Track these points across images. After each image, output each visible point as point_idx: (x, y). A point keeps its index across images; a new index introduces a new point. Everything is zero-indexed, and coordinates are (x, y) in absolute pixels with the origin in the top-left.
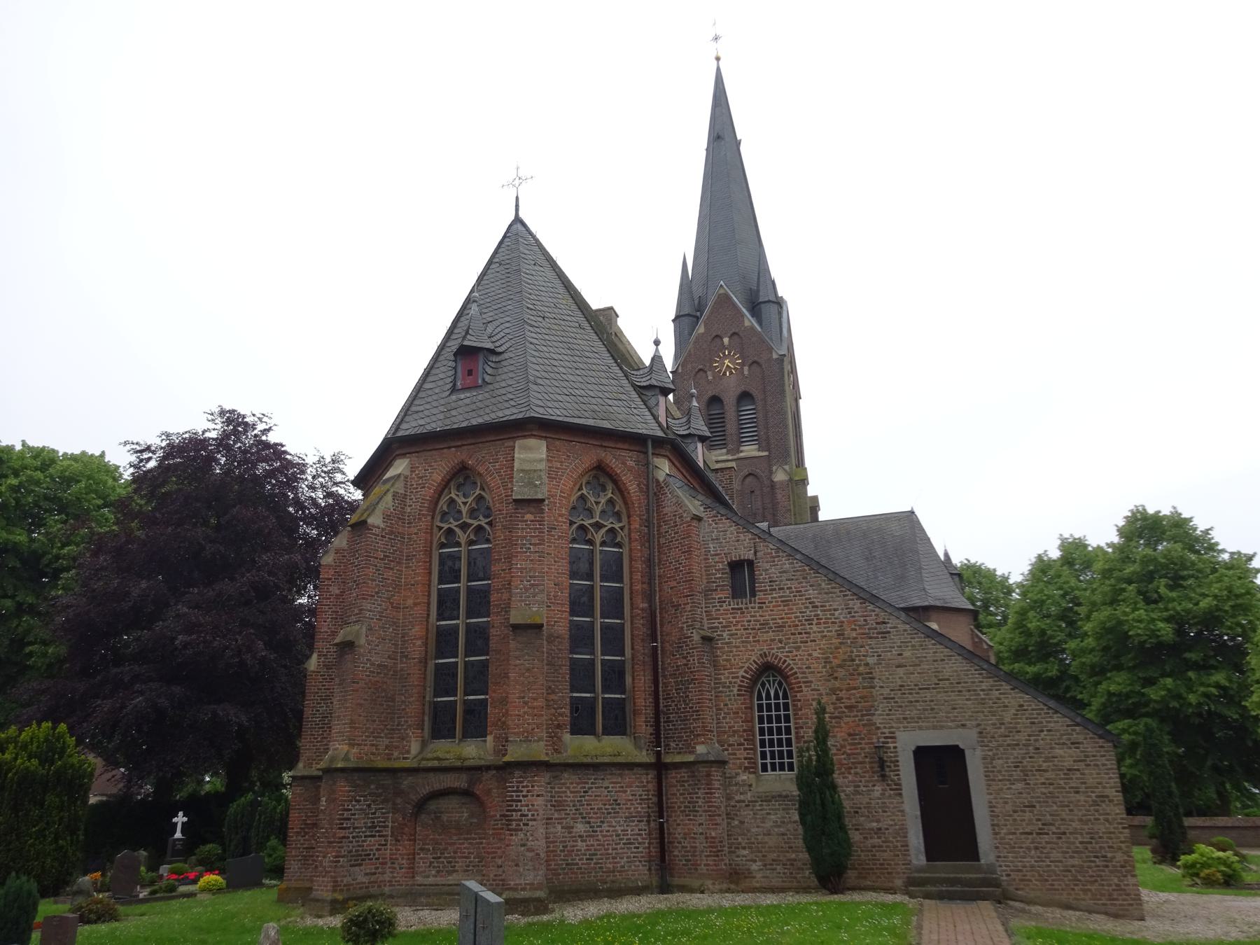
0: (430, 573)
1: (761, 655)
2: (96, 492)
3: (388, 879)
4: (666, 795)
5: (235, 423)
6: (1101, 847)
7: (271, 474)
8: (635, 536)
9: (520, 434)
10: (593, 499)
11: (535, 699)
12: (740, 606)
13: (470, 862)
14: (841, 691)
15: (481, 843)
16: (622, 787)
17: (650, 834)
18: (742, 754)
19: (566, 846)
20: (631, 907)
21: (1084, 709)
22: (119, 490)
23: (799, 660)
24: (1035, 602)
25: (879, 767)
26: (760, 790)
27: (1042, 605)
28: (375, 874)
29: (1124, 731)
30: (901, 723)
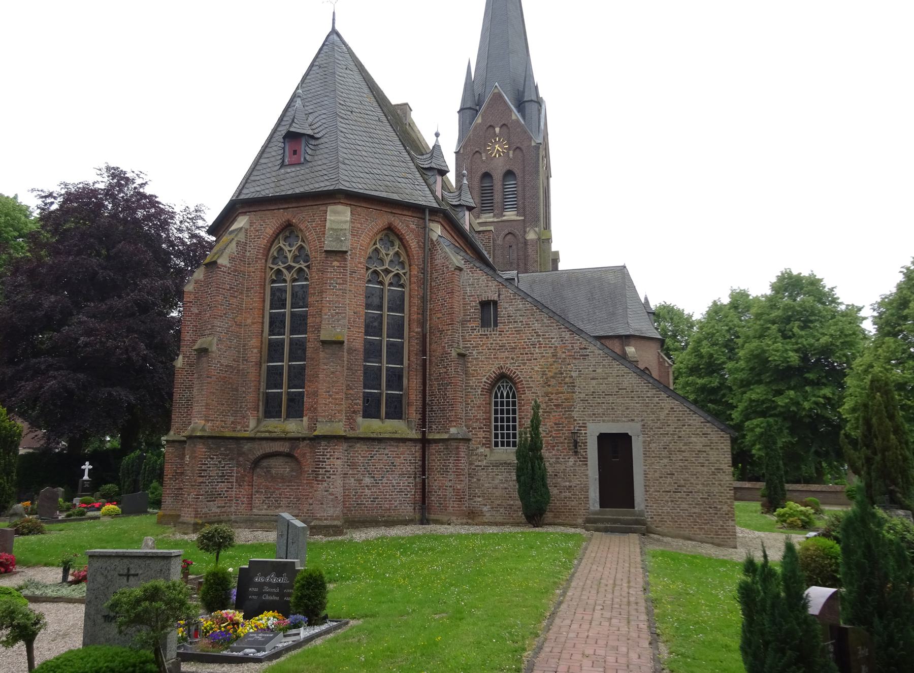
0: (264, 301)
1: (498, 368)
2: (12, 226)
3: (234, 510)
4: (428, 460)
5: (119, 178)
6: (714, 502)
7: (148, 218)
8: (414, 279)
9: (331, 202)
10: (384, 252)
11: (337, 393)
12: (486, 333)
13: (291, 501)
14: (552, 394)
15: (299, 489)
16: (398, 454)
17: (415, 486)
18: (481, 434)
19: (357, 492)
20: (399, 533)
21: (733, 410)
22: (30, 225)
23: (525, 372)
24: (708, 334)
25: (573, 446)
26: (492, 459)
27: (712, 337)
28: (225, 507)
29: (757, 425)
30: (591, 417)
